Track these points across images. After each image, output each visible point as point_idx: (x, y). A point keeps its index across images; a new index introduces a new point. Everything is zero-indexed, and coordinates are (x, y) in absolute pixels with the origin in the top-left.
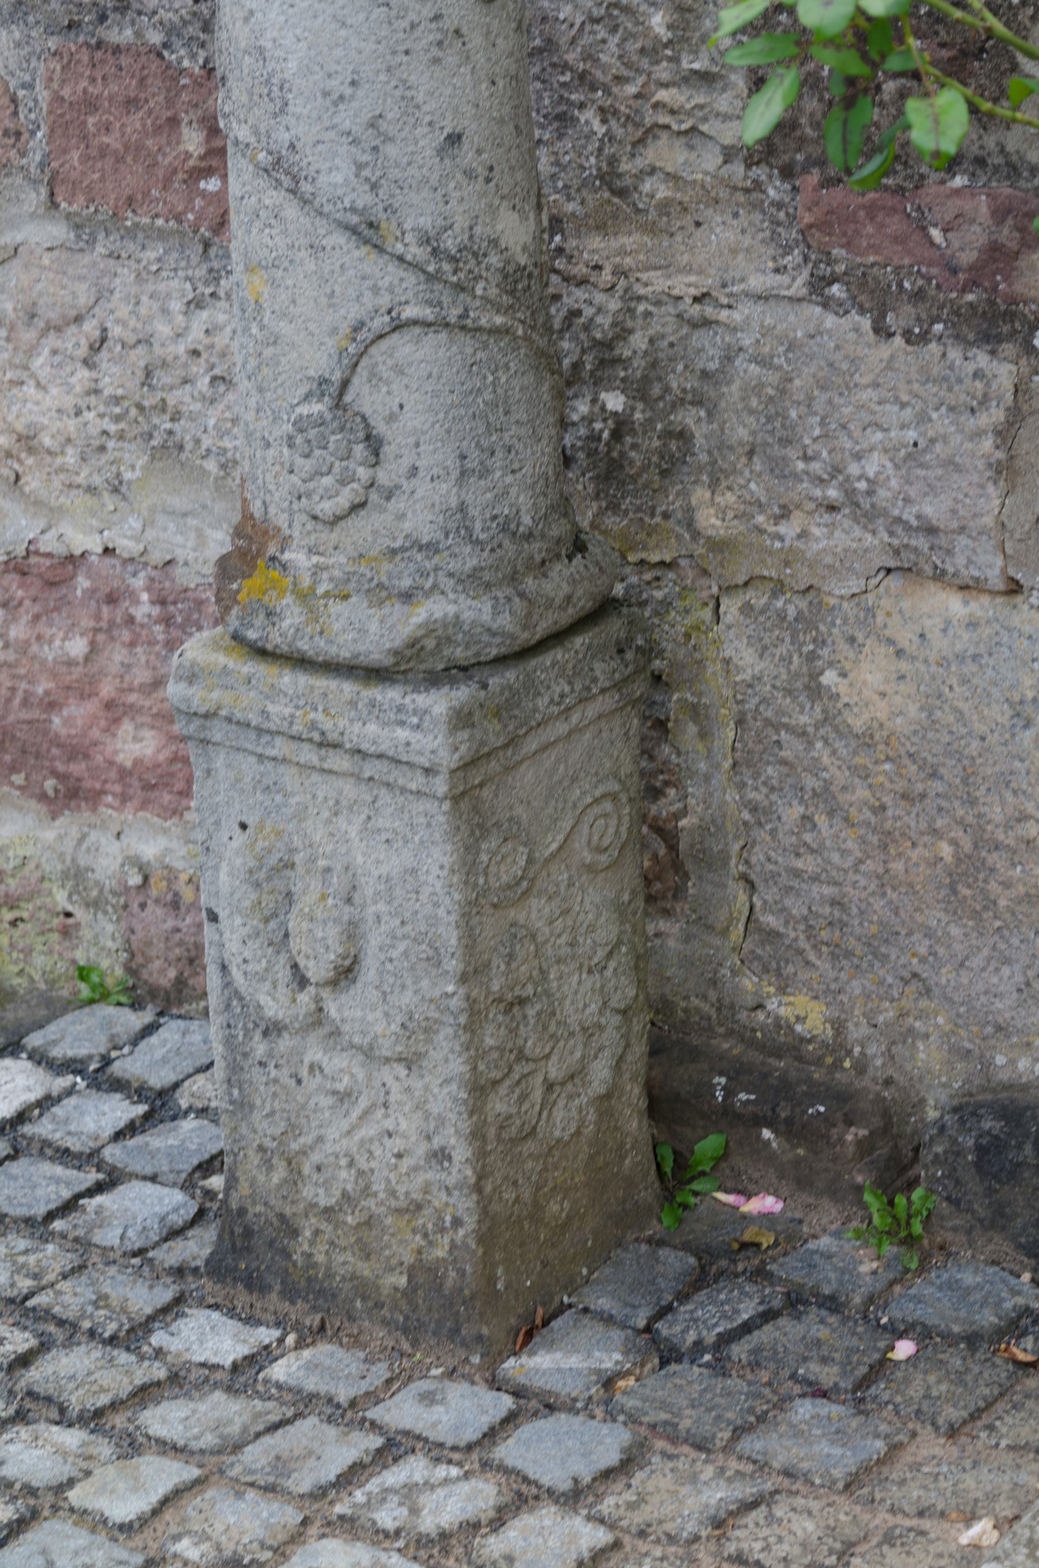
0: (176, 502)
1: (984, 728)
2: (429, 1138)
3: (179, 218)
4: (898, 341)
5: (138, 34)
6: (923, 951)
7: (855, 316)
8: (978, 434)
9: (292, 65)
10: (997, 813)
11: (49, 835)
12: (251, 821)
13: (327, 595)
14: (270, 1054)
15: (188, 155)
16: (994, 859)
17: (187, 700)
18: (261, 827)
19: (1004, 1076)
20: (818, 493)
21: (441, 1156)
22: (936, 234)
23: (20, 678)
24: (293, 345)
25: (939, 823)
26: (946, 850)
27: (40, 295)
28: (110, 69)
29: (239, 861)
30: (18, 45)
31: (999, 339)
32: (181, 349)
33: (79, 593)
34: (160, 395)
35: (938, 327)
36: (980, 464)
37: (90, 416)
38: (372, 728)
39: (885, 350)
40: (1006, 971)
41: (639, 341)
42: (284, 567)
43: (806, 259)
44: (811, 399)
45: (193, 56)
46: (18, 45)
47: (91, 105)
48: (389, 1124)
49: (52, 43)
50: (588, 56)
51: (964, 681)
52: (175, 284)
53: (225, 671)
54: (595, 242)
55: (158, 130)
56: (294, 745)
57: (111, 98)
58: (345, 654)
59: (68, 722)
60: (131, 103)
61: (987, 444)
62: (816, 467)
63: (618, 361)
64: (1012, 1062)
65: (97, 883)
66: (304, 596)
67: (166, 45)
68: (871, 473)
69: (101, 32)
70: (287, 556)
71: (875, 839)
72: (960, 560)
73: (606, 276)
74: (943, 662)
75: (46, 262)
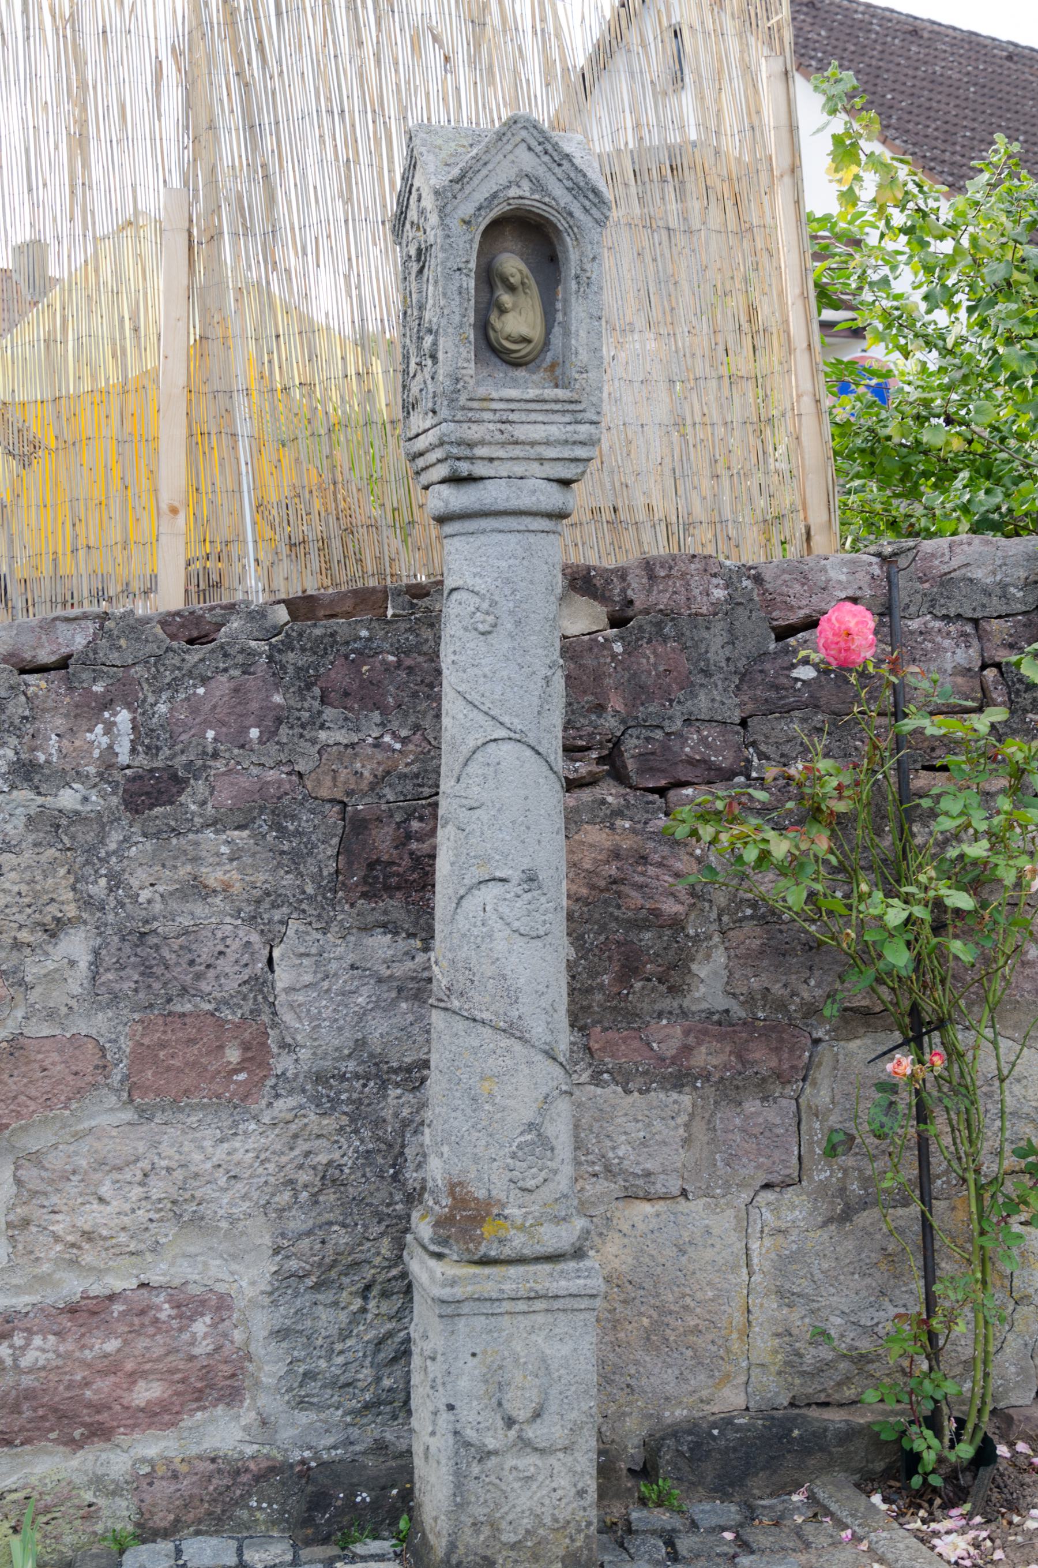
0: (192, 1250)
1: (663, 1261)
2: (575, 1485)
3: (218, 1097)
4: (636, 1094)
5: (195, 1006)
6: (633, 1372)
7: (613, 1087)
8: (677, 1127)
9: (522, 980)
10: (670, 1298)
11: (75, 1463)
12: (477, 1351)
13: (531, 1226)
14: (482, 1472)
15: (229, 1063)
16: (669, 1319)
17: (453, 1295)
18: (485, 1352)
19: (669, 1421)
20: (590, 1169)
21: (581, 1493)
22: (655, 1045)
23: (66, 1373)
24: (515, 1110)
25: (642, 1309)
26: (646, 1321)
27: (109, 1152)
28: (178, 1025)
29: (476, 1372)
30: (110, 1020)
31: (683, 1086)
32: (208, 1165)
33: (115, 1315)
34: (190, 1193)
35: (654, 1085)
36: (678, 1140)
37: (140, 1212)
38: (563, 1283)
39: (630, 1099)
40: (669, 1371)
42: (506, 1218)
43: (591, 1065)
44: (591, 1126)
45: (234, 1013)
47: (163, 1045)
48: (554, 1485)
49: (136, 1016)
51: (654, 1241)
52: (209, 1132)
53: (475, 1276)
55: (209, 1053)
56: (513, 1303)
57: (177, 1041)
58: (551, 1250)
59: (96, 1392)
60: (191, 1041)
61: (681, 1131)
62: (590, 1157)
64: (673, 1413)
65: (113, 1481)
66: (522, 1228)
67: (216, 1010)
68: (621, 1154)
69: (170, 1007)
70: (506, 1212)
71: (609, 1326)
72: (659, 1186)
74: (644, 1235)
75: (114, 1134)
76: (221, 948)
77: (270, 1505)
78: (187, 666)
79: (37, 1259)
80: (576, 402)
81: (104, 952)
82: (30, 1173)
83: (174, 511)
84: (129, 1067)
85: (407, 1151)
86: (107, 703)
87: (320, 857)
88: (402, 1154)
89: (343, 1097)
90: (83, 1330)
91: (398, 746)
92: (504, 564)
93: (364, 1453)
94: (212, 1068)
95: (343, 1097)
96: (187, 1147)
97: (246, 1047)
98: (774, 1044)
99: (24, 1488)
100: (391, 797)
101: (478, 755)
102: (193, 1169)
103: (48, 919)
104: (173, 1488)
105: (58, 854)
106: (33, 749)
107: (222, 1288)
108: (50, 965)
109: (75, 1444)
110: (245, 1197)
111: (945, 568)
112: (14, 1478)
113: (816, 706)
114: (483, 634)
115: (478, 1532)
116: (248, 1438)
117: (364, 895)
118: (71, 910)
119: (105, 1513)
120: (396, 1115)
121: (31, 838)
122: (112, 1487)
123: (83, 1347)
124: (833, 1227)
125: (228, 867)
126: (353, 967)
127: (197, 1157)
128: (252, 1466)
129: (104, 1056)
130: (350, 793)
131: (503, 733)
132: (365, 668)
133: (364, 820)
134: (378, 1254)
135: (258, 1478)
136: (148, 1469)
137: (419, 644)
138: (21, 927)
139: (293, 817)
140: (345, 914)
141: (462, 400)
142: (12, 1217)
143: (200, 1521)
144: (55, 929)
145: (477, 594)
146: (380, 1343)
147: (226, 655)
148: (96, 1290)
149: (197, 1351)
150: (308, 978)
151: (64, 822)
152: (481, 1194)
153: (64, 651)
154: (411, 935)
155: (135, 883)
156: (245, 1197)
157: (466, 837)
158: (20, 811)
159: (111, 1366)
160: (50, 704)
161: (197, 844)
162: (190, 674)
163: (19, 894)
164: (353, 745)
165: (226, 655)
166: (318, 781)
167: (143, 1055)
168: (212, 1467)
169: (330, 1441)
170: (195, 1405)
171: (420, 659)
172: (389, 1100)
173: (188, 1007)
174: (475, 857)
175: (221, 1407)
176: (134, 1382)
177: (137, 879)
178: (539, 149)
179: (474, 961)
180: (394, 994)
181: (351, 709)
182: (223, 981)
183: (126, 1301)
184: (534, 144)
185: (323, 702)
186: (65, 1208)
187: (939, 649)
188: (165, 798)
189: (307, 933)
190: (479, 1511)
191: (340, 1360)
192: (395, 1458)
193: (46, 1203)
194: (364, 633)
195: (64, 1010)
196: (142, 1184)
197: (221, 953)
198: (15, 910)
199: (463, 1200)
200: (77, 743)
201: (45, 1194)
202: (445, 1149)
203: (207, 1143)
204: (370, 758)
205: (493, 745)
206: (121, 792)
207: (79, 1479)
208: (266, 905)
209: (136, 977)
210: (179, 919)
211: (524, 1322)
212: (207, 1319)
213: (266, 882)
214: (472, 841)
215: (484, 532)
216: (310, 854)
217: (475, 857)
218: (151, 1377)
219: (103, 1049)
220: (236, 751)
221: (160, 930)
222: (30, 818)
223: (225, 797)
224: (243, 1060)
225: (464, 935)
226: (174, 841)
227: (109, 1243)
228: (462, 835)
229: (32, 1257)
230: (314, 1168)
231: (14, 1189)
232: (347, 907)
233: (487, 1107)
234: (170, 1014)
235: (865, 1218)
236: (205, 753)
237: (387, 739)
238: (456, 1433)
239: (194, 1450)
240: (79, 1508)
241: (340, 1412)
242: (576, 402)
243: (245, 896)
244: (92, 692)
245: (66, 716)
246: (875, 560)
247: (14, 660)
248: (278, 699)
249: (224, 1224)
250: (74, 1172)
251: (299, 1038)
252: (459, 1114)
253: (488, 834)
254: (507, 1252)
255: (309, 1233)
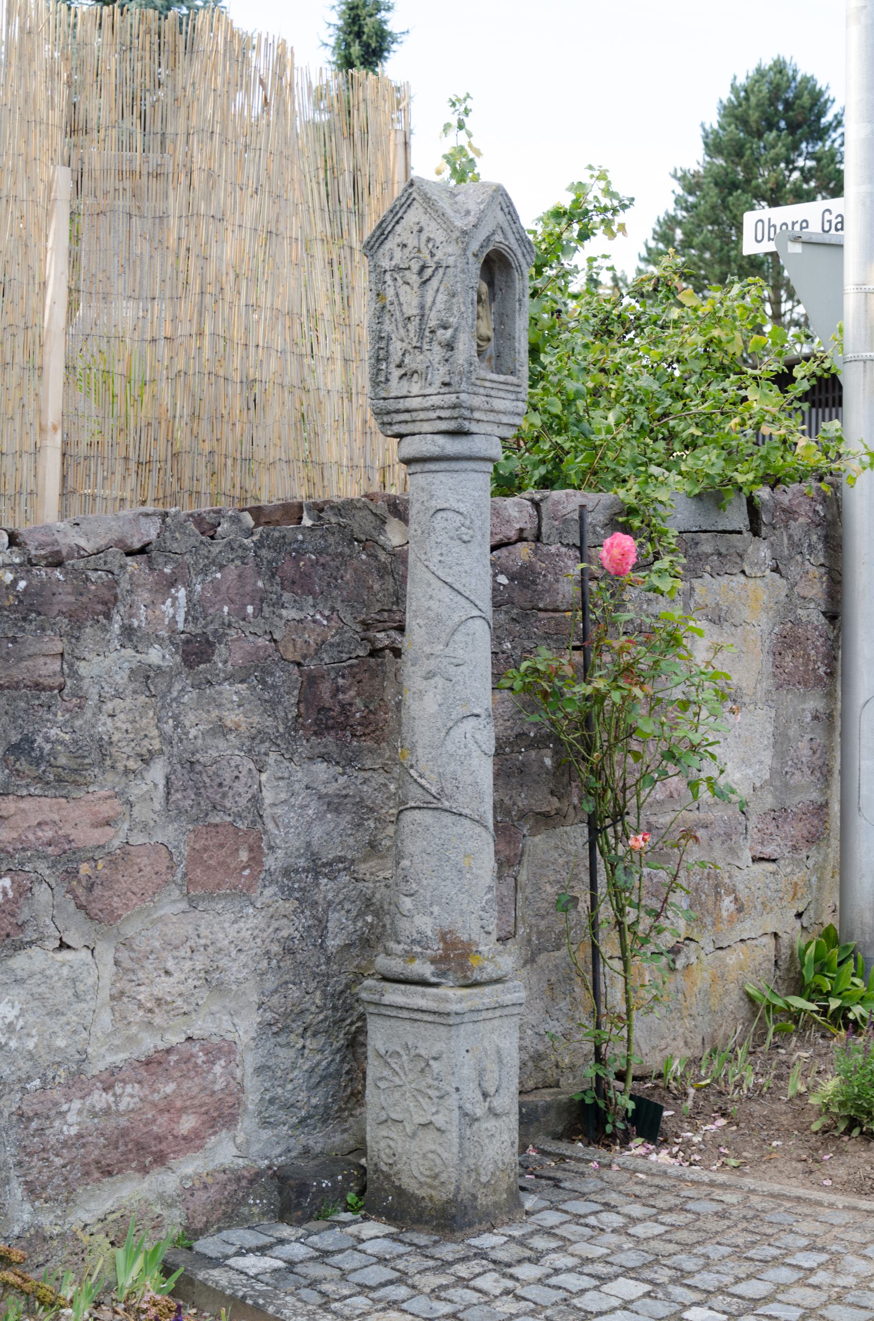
11: (145, 1185)
21: (513, 1143)
30: (176, 830)
41: (378, 896)
46: (176, 830)
50: (373, 802)
54: (363, 866)
57: (214, 845)
59: (160, 1126)
60: (222, 846)
63: (372, 904)
65: (170, 1196)
73: (368, 876)
76: (236, 773)
77: (261, 1201)
78: (212, 556)
79: (129, 1023)
80: (518, 386)
81: (173, 777)
82: (124, 955)
83: (55, 428)
84: (186, 866)
85: (329, 925)
86: (173, 584)
87: (286, 704)
88: (326, 927)
89: (296, 886)
90: (154, 1077)
91: (325, 622)
92: (476, 494)
93: (295, 1158)
94: (232, 866)
95: (296, 886)
96: (216, 928)
97: (251, 850)
98: (508, 839)
99: (119, 1209)
100: (327, 660)
101: (462, 628)
102: (219, 945)
103: (144, 751)
104: (206, 1196)
105: (147, 700)
106: (131, 616)
107: (229, 1037)
108: (145, 788)
109: (144, 1170)
110: (245, 966)
111: (565, 512)
112: (110, 1202)
113: (513, 603)
114: (465, 542)
115: (469, 1177)
116: (239, 1154)
117: (315, 733)
118: (157, 745)
119: (166, 1222)
120: (325, 898)
121: (131, 687)
122: (169, 1201)
123: (154, 1091)
124: (528, 967)
125: (237, 712)
126: (307, 787)
127: (221, 936)
128: (246, 1174)
129: (172, 859)
130: (304, 657)
131: (476, 613)
132: (302, 563)
133: (315, 677)
134: (314, 1003)
135: (251, 1182)
136: (190, 1184)
137: (327, 547)
138: (129, 757)
139: (272, 674)
140: (303, 748)
141: (473, 377)
142: (114, 991)
143: (219, 1220)
144: (146, 760)
145: (461, 514)
146: (312, 1070)
147: (232, 549)
148: (162, 1046)
149: (217, 1087)
150: (283, 796)
151: (152, 674)
152: (465, 938)
153: (146, 539)
154: (338, 763)
155: (187, 723)
156: (245, 966)
157: (453, 686)
158: (126, 665)
159: (167, 1107)
160: (141, 581)
161: (221, 693)
162: (213, 563)
163: (127, 731)
164: (300, 621)
165: (232, 549)
166: (285, 646)
167: (196, 857)
168: (225, 1177)
169: (278, 1150)
170: (211, 1131)
171: (328, 558)
172: (321, 887)
173: (217, 820)
174: (460, 700)
175: (225, 1131)
176: (180, 1117)
177: (189, 719)
178: (506, 210)
179: (459, 773)
180: (325, 808)
181: (297, 594)
182: (237, 799)
183: (178, 1053)
184: (504, 206)
185: (283, 589)
186: (146, 981)
187: (566, 567)
188: (205, 657)
189: (281, 762)
190: (471, 1161)
191: (289, 1087)
192: (314, 1159)
193: (134, 978)
194: (300, 537)
195: (152, 823)
196: (191, 959)
197: (237, 777)
198: (124, 743)
199: (453, 943)
200: (157, 612)
201: (133, 971)
202: (436, 909)
203: (227, 925)
204: (313, 630)
205: (471, 621)
206: (180, 651)
207: (152, 1197)
208: (257, 741)
209: (193, 797)
210: (210, 752)
211: (489, 1025)
212: (222, 1062)
213: (258, 723)
214: (458, 688)
215: (465, 471)
216: (280, 702)
217: (460, 700)
218: (190, 1111)
219: (171, 853)
220: (242, 623)
221: (201, 760)
222: (132, 670)
223: (238, 658)
224: (249, 859)
225: (451, 755)
226: (208, 691)
227: (169, 1007)
228: (449, 684)
229: (125, 1022)
230: (278, 941)
231: (114, 969)
232: (304, 742)
233: (468, 876)
234: (209, 825)
235: (542, 959)
236: (223, 623)
237: (318, 617)
238: (460, 1108)
239: (211, 1167)
240: (152, 1219)
241: (286, 1128)
242: (518, 386)
243: (248, 734)
244: (164, 573)
245: (150, 591)
246: (529, 503)
247: (121, 545)
248: (260, 584)
249: (234, 987)
250: (152, 952)
251: (277, 841)
252: (448, 882)
253: (468, 683)
254: (485, 977)
255: (276, 991)
